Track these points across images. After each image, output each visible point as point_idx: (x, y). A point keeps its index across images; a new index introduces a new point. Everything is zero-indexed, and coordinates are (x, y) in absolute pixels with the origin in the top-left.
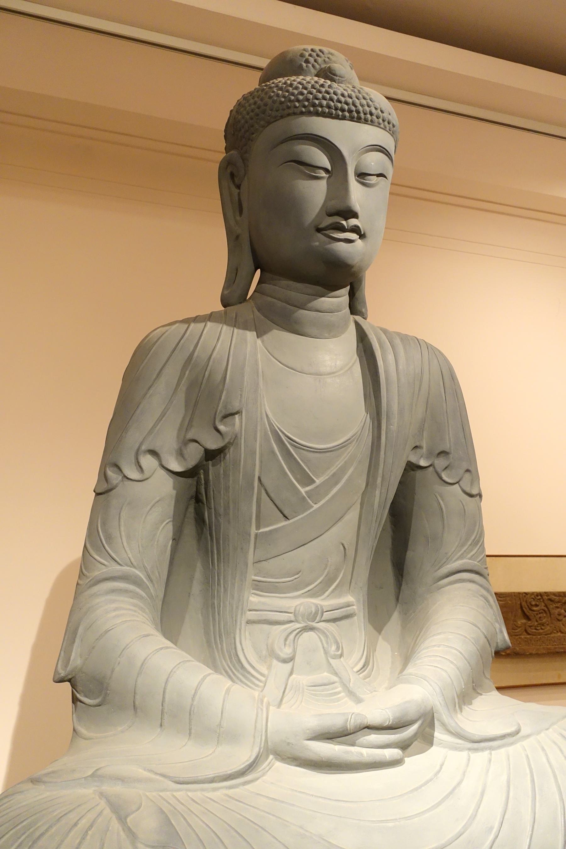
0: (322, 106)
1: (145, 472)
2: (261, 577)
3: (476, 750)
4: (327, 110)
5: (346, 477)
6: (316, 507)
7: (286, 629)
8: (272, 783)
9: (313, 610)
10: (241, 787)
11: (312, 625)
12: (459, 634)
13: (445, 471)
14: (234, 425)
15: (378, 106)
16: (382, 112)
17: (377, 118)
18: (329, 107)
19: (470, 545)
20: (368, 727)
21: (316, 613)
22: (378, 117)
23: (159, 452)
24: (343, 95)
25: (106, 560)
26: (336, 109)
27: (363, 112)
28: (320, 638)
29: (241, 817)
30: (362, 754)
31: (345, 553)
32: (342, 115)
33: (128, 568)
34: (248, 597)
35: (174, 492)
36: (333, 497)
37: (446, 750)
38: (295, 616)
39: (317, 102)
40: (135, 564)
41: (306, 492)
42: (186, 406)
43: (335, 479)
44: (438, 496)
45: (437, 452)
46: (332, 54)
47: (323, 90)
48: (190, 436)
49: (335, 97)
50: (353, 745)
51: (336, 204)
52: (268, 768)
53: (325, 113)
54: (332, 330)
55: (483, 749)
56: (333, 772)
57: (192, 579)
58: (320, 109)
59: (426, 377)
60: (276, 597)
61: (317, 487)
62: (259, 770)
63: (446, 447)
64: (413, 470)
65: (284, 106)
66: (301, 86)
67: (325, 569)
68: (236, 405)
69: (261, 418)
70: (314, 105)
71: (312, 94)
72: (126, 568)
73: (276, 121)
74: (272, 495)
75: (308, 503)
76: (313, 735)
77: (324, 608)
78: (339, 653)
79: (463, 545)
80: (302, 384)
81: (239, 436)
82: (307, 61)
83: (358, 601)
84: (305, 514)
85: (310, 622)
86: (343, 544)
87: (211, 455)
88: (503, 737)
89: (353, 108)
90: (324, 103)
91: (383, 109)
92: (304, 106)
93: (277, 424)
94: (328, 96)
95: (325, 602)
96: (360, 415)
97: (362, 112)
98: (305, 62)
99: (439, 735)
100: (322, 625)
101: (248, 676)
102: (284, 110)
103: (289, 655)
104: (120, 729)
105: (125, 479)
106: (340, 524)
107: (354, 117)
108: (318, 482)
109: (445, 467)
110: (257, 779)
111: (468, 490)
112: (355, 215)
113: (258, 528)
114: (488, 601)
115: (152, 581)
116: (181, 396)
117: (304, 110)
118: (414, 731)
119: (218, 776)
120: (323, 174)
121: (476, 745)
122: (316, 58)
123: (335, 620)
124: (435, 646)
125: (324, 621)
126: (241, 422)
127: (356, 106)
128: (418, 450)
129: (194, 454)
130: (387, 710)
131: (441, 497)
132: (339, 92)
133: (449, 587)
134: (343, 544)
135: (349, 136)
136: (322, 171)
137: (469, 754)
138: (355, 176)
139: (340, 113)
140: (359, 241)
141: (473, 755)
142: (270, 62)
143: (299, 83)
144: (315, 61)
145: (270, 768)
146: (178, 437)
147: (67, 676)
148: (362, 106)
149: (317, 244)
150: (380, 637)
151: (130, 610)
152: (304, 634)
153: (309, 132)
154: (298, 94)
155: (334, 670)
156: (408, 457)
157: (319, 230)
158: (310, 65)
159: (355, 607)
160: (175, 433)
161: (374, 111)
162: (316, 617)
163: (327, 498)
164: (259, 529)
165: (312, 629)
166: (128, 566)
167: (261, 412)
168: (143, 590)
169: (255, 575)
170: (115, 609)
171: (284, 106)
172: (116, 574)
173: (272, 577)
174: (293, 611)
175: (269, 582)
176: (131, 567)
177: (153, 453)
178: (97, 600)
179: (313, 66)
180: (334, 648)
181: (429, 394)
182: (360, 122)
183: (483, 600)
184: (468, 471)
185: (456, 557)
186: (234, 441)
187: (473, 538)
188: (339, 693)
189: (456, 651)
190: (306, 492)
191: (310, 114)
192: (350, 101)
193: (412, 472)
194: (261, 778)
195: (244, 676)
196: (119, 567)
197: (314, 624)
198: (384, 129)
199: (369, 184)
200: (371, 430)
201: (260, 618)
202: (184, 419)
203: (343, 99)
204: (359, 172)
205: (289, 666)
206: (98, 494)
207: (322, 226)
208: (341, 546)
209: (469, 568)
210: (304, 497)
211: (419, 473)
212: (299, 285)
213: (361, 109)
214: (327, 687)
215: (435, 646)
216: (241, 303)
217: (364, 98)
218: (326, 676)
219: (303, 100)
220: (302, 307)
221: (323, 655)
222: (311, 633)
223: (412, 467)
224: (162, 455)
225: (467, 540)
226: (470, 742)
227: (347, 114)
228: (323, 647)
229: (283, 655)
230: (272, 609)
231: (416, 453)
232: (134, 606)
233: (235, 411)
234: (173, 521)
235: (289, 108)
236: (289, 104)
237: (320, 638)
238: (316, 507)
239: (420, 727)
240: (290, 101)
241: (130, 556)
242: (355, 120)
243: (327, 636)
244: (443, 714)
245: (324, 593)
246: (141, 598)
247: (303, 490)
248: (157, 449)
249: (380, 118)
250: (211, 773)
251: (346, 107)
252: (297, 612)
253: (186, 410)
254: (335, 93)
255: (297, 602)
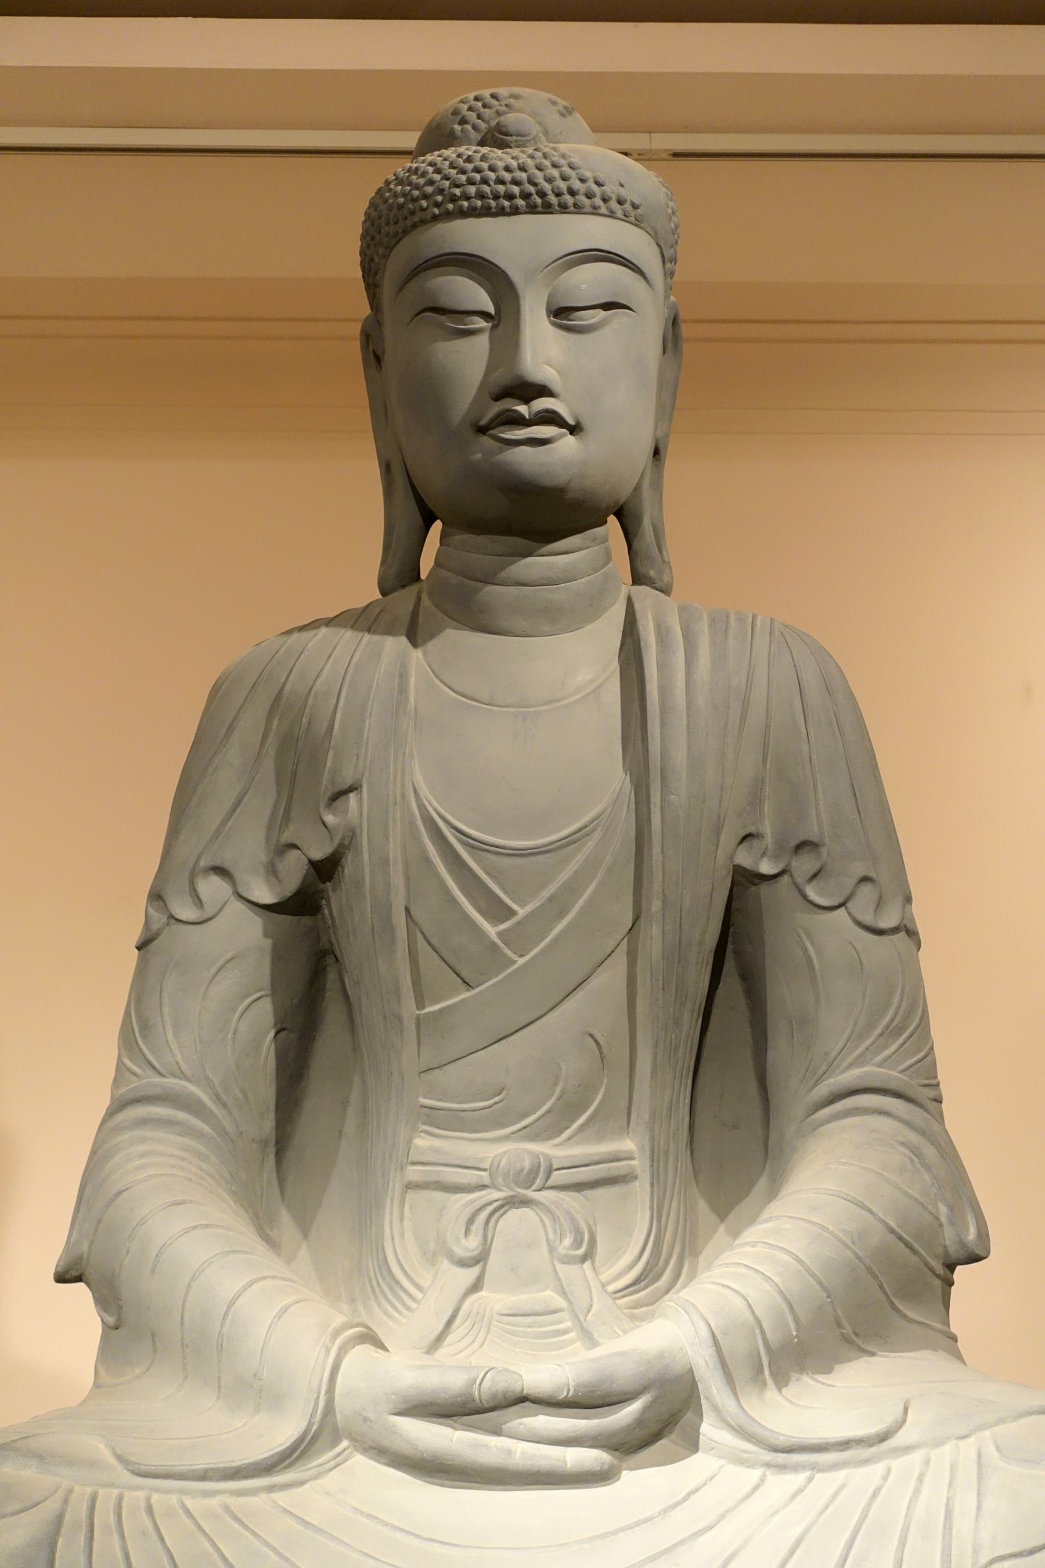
0: (468, 198)
1: (206, 907)
2: (434, 1099)
3: (782, 1468)
4: (479, 203)
5: (581, 902)
6: (521, 961)
7: (472, 1202)
8: (327, 1493)
9: (527, 1164)
10: (263, 1496)
11: (525, 1195)
12: (810, 1222)
13: (814, 883)
14: (346, 811)
15: (588, 174)
16: (599, 184)
17: (589, 198)
18: (482, 196)
19: (881, 1035)
20: (523, 1399)
21: (534, 1172)
22: (589, 196)
23: (232, 870)
24: (507, 169)
25: (139, 1067)
26: (496, 197)
27: (553, 192)
28: (542, 1221)
29: (211, 1549)
30: (509, 1452)
31: (601, 1053)
32: (510, 206)
33: (176, 1081)
34: (411, 1139)
35: (268, 943)
36: (555, 941)
37: (722, 1462)
38: (491, 1176)
39: (457, 192)
40: (188, 1072)
41: (499, 934)
42: (278, 783)
43: (557, 906)
44: (804, 937)
45: (794, 843)
46: (516, 97)
47: (470, 166)
48: (286, 837)
49: (492, 176)
50: (497, 1432)
51: (502, 377)
52: (332, 1463)
53: (475, 209)
54: (557, 619)
55: (796, 1468)
56: (464, 1484)
57: (345, 1103)
58: (466, 204)
59: (759, 694)
60: (481, 1140)
61: (519, 923)
62: (307, 1467)
63: (812, 832)
64: (755, 884)
65: (405, 212)
66: (431, 169)
67: (555, 1085)
68: (348, 777)
69: (403, 796)
70: (453, 199)
71: (448, 179)
72: (170, 1082)
73: (399, 241)
74: (434, 942)
75: (504, 955)
76: (404, 1406)
77: (554, 1162)
78: (581, 1251)
79: (861, 1037)
80: (516, 730)
81: (358, 831)
82: (463, 121)
83: (642, 1149)
84: (501, 977)
85: (524, 1186)
86: (591, 1036)
87: (326, 870)
88: (845, 1445)
89: (532, 189)
90: (472, 190)
91: (601, 177)
92: (437, 205)
93: (434, 805)
94: (477, 177)
95: (555, 1150)
96: (616, 779)
97: (550, 192)
98: (459, 124)
99: (709, 1429)
100: (547, 1196)
101: (397, 1289)
102: (406, 219)
103: (473, 1250)
104: (137, 1371)
105: (173, 921)
106: (580, 994)
107: (536, 206)
108: (521, 912)
109: (811, 874)
110: (303, 1483)
111: (868, 919)
112: (544, 391)
113: (420, 1004)
114: (920, 1156)
115: (224, 1105)
116: (269, 765)
117: (436, 211)
118: (658, 1419)
119: (213, 1469)
120: (481, 323)
121: (781, 1458)
122: (482, 110)
123: (579, 1187)
124: (747, 1244)
125: (552, 1188)
126: (361, 806)
127: (535, 184)
128: (755, 842)
129: (294, 872)
130: (566, 1367)
131: (809, 936)
132: (500, 164)
133: (832, 1125)
134: (591, 1036)
135: (505, 240)
136: (477, 319)
137: (764, 1475)
138: (548, 317)
139: (506, 203)
140: (570, 439)
141: (772, 1478)
142: (421, 138)
143: (431, 164)
144: (479, 117)
145: (336, 1467)
146: (267, 841)
147: (68, 1271)
148: (549, 180)
149: (479, 456)
150: (722, 1228)
151: (172, 1156)
152: (509, 1213)
153: (448, 251)
154: (424, 185)
155: (561, 1285)
156: (732, 857)
157: (482, 430)
158: (469, 127)
159: (635, 1162)
160: (261, 834)
161: (577, 185)
162: (535, 1178)
163: (542, 945)
164: (424, 1008)
165: (526, 1202)
166: (175, 1077)
167: (403, 786)
168: (205, 1120)
169: (425, 1097)
170: (143, 1155)
171: (405, 212)
172: (152, 1092)
173: (453, 1101)
174: (487, 1166)
175: (449, 1110)
176: (180, 1079)
177: (220, 871)
178: (119, 1139)
179: (474, 127)
180: (568, 1241)
181: (767, 726)
182: (551, 213)
183: (907, 1152)
184: (865, 879)
185: (849, 1060)
186: (350, 842)
187: (886, 1020)
188: (565, 1332)
189: (786, 1257)
190: (499, 934)
191: (448, 216)
192: (524, 176)
193: (754, 888)
194: (311, 1483)
195: (391, 1288)
196: (158, 1079)
197: (530, 1193)
198: (612, 215)
199: (580, 326)
200: (633, 806)
201: (427, 1179)
202: (276, 807)
203: (507, 176)
204: (554, 308)
205: (473, 1272)
206: (139, 948)
207: (484, 422)
208: (590, 1039)
209: (877, 1084)
210: (494, 944)
211: (764, 889)
212: (482, 540)
213: (547, 187)
214: (541, 1318)
215: (747, 1244)
216: (404, 587)
217: (555, 166)
218: (550, 1296)
219: (433, 194)
220: (490, 579)
221: (546, 1255)
222: (526, 1212)
223: (744, 880)
224: (237, 876)
225: (871, 1025)
226: (769, 1451)
227: (520, 202)
228: (548, 1240)
229: (459, 1252)
230: (450, 1162)
231: (751, 848)
232: (184, 1150)
233: (345, 787)
234: (273, 994)
235: (413, 213)
236: (410, 206)
237: (542, 1221)
238: (521, 961)
239: (645, 1409)
240: (415, 200)
241: (179, 1058)
242: (540, 209)
243: (555, 1219)
244: (712, 1386)
245: (561, 1132)
246: (200, 1135)
247: (492, 930)
248: (227, 865)
249: (610, 198)
250: (202, 1462)
251: (516, 190)
252: (494, 1168)
253: (279, 793)
254: (492, 169)
255: (500, 1150)
